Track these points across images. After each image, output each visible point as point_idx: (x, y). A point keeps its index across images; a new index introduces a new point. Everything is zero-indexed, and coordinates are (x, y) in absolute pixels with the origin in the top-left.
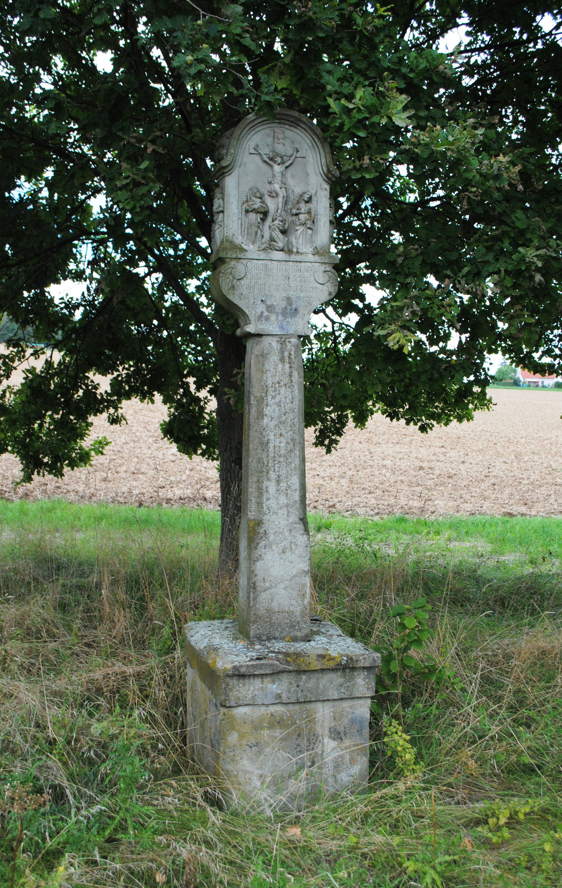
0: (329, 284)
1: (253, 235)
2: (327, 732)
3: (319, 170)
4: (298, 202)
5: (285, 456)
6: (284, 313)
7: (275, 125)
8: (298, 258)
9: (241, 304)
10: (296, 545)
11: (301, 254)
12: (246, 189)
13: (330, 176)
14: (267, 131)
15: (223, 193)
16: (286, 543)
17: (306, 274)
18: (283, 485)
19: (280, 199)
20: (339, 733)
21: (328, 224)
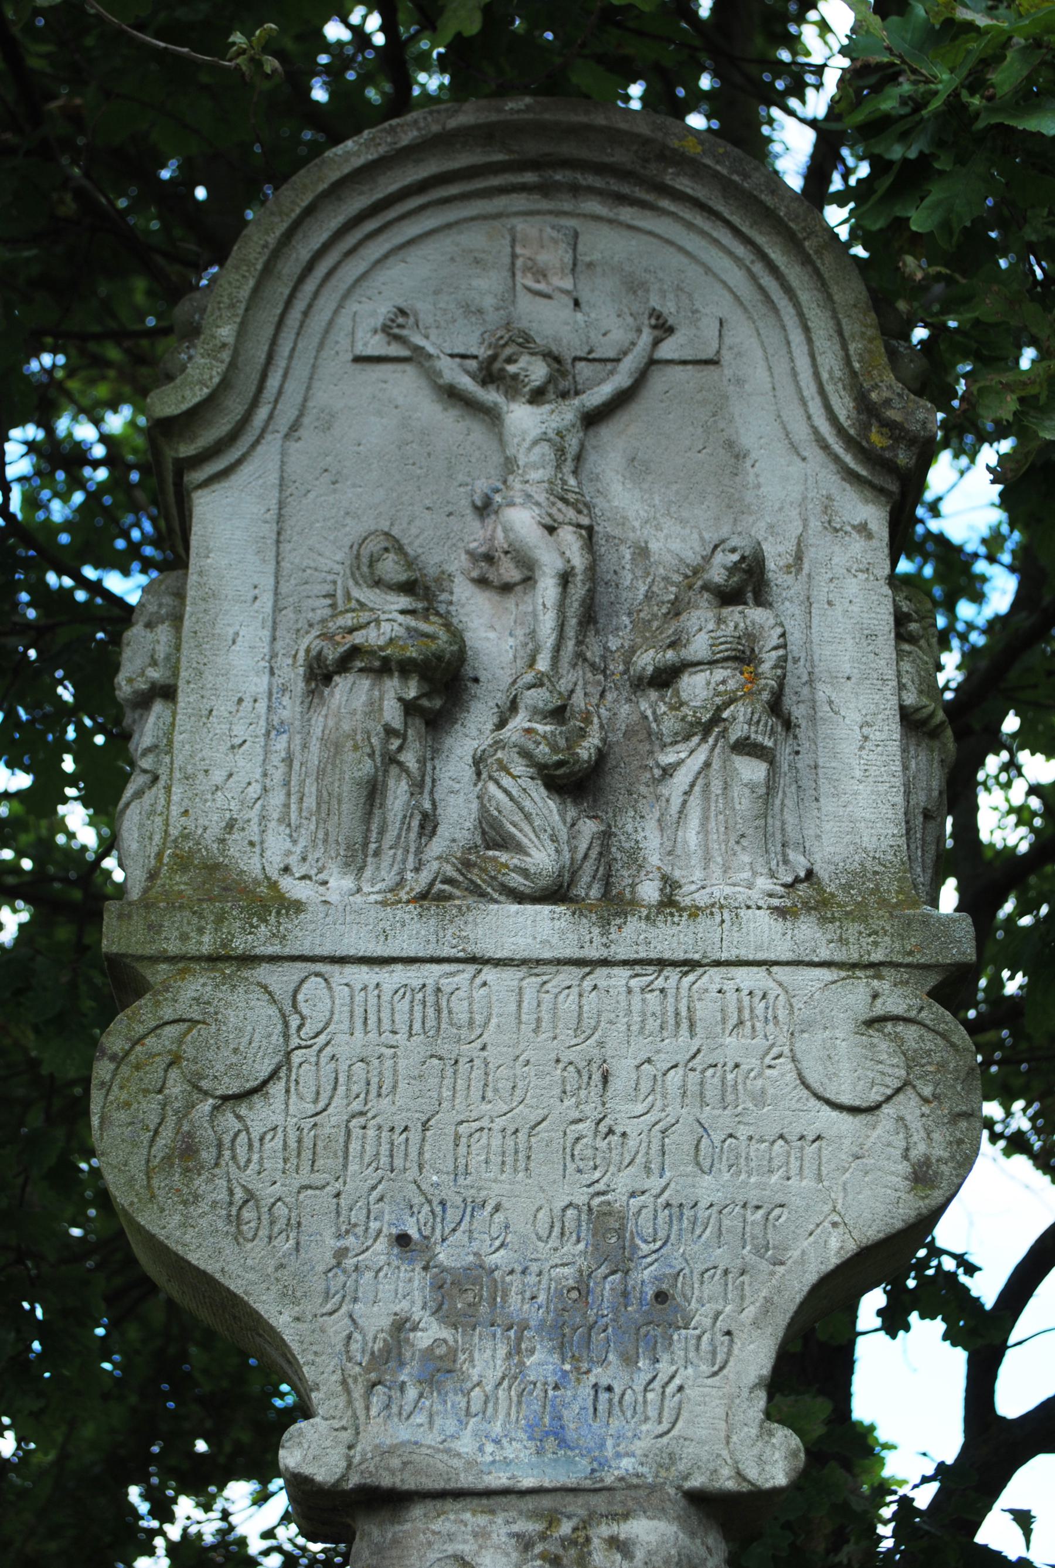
0: (908, 1106)
1: (349, 807)
3: (805, 419)
4: (676, 609)
6: (573, 1327)
7: (519, 202)
8: (670, 939)
9: (242, 1269)
11: (695, 911)
12: (333, 558)
13: (877, 439)
14: (474, 238)
17: (733, 1045)
19: (548, 588)
21: (889, 731)
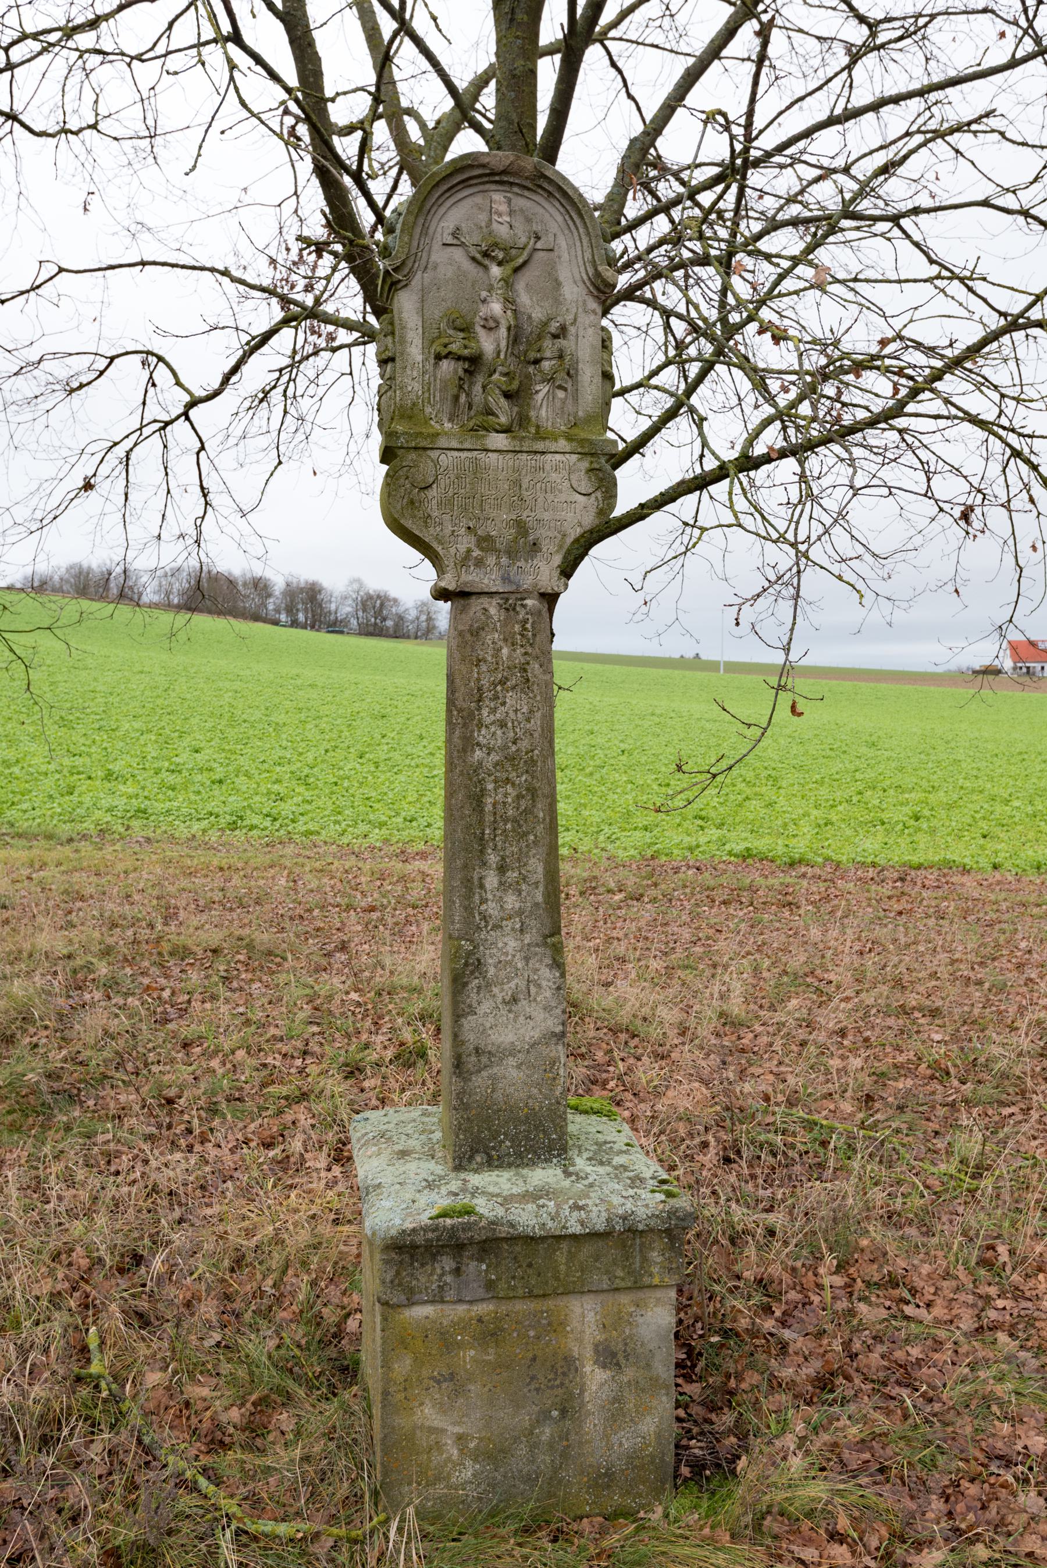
2: (589, 1352)
5: (515, 821)
10: (539, 986)
14: (478, 199)
16: (519, 982)
18: (512, 875)
19: (503, 332)
20: (614, 1355)
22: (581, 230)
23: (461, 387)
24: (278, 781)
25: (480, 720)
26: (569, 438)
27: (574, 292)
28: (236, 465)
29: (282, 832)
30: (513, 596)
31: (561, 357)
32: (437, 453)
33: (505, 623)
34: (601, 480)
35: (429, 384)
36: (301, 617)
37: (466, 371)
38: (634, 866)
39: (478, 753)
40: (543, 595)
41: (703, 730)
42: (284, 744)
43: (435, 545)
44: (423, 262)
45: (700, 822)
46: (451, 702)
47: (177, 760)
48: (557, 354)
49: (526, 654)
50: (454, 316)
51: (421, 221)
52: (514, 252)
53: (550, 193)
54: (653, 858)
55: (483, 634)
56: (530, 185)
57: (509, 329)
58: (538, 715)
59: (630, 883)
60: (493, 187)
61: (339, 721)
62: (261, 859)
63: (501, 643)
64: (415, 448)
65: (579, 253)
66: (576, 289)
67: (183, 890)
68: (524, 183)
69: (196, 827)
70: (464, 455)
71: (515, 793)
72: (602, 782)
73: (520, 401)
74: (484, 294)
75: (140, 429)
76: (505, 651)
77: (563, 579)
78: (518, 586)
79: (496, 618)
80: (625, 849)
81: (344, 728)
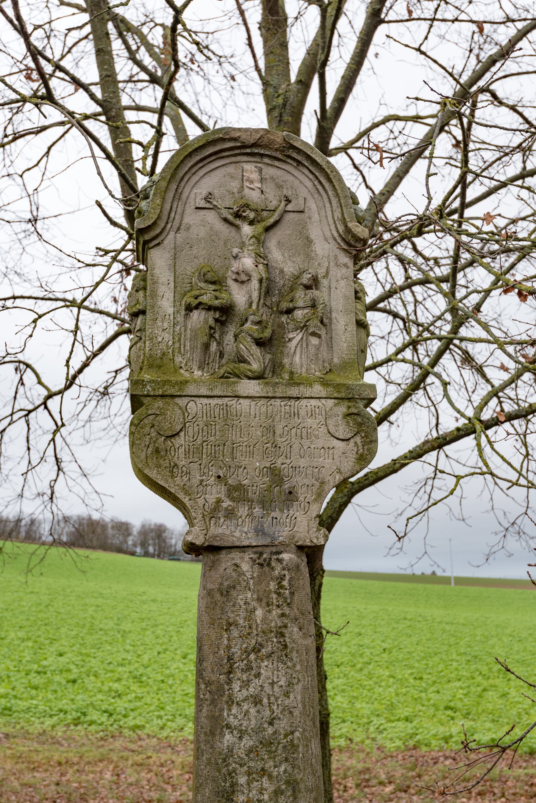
14: (231, 169)
15: (192, 561)
19: (255, 284)
22: (330, 193)
23: (211, 336)
24: (119, 680)
25: (230, 697)
26: (325, 384)
27: (325, 248)
28: (82, 441)
29: (115, 726)
30: (268, 550)
31: (313, 306)
32: (186, 400)
33: (259, 581)
34: (360, 425)
35: (180, 334)
36: (151, 549)
37: (217, 320)
38: (400, 757)
39: (228, 737)
40: (300, 548)
41: (444, 631)
42: (128, 647)
43: (181, 496)
44: (176, 224)
45: (449, 712)
46: (200, 674)
47: (45, 663)
48: (309, 303)
49: (283, 615)
50: (205, 270)
51: (174, 186)
52: (265, 214)
53: (299, 163)
54: (415, 748)
55: (234, 593)
56: (280, 156)
57: (261, 281)
58: (299, 688)
59: (398, 774)
60: (245, 158)
61: (170, 629)
62: (94, 754)
63: (254, 604)
64: (162, 396)
65: (329, 213)
66: (327, 246)
67: (26, 785)
68: (274, 154)
69: (49, 722)
70: (214, 402)
71: (272, 788)
72: (370, 676)
73: (274, 349)
74: (235, 250)
75: (11, 415)
76: (259, 613)
77: (323, 530)
78: (273, 538)
79: (248, 575)
80: (391, 739)
81: (173, 634)
